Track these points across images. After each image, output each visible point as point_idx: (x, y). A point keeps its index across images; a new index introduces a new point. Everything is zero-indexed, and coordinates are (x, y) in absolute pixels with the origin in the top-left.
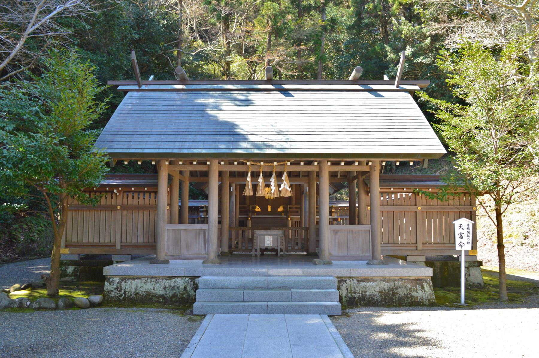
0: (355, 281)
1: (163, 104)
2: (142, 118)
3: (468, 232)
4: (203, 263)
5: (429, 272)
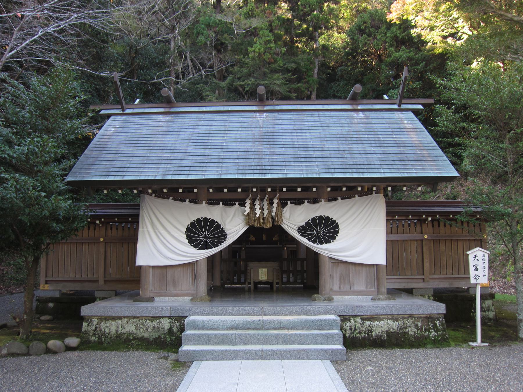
0: (359, 320)
1: (147, 128)
2: (124, 142)
3: (484, 263)
4: (192, 300)
5: (440, 308)
